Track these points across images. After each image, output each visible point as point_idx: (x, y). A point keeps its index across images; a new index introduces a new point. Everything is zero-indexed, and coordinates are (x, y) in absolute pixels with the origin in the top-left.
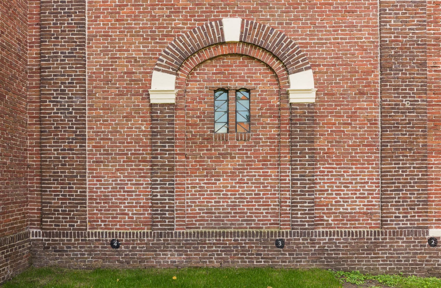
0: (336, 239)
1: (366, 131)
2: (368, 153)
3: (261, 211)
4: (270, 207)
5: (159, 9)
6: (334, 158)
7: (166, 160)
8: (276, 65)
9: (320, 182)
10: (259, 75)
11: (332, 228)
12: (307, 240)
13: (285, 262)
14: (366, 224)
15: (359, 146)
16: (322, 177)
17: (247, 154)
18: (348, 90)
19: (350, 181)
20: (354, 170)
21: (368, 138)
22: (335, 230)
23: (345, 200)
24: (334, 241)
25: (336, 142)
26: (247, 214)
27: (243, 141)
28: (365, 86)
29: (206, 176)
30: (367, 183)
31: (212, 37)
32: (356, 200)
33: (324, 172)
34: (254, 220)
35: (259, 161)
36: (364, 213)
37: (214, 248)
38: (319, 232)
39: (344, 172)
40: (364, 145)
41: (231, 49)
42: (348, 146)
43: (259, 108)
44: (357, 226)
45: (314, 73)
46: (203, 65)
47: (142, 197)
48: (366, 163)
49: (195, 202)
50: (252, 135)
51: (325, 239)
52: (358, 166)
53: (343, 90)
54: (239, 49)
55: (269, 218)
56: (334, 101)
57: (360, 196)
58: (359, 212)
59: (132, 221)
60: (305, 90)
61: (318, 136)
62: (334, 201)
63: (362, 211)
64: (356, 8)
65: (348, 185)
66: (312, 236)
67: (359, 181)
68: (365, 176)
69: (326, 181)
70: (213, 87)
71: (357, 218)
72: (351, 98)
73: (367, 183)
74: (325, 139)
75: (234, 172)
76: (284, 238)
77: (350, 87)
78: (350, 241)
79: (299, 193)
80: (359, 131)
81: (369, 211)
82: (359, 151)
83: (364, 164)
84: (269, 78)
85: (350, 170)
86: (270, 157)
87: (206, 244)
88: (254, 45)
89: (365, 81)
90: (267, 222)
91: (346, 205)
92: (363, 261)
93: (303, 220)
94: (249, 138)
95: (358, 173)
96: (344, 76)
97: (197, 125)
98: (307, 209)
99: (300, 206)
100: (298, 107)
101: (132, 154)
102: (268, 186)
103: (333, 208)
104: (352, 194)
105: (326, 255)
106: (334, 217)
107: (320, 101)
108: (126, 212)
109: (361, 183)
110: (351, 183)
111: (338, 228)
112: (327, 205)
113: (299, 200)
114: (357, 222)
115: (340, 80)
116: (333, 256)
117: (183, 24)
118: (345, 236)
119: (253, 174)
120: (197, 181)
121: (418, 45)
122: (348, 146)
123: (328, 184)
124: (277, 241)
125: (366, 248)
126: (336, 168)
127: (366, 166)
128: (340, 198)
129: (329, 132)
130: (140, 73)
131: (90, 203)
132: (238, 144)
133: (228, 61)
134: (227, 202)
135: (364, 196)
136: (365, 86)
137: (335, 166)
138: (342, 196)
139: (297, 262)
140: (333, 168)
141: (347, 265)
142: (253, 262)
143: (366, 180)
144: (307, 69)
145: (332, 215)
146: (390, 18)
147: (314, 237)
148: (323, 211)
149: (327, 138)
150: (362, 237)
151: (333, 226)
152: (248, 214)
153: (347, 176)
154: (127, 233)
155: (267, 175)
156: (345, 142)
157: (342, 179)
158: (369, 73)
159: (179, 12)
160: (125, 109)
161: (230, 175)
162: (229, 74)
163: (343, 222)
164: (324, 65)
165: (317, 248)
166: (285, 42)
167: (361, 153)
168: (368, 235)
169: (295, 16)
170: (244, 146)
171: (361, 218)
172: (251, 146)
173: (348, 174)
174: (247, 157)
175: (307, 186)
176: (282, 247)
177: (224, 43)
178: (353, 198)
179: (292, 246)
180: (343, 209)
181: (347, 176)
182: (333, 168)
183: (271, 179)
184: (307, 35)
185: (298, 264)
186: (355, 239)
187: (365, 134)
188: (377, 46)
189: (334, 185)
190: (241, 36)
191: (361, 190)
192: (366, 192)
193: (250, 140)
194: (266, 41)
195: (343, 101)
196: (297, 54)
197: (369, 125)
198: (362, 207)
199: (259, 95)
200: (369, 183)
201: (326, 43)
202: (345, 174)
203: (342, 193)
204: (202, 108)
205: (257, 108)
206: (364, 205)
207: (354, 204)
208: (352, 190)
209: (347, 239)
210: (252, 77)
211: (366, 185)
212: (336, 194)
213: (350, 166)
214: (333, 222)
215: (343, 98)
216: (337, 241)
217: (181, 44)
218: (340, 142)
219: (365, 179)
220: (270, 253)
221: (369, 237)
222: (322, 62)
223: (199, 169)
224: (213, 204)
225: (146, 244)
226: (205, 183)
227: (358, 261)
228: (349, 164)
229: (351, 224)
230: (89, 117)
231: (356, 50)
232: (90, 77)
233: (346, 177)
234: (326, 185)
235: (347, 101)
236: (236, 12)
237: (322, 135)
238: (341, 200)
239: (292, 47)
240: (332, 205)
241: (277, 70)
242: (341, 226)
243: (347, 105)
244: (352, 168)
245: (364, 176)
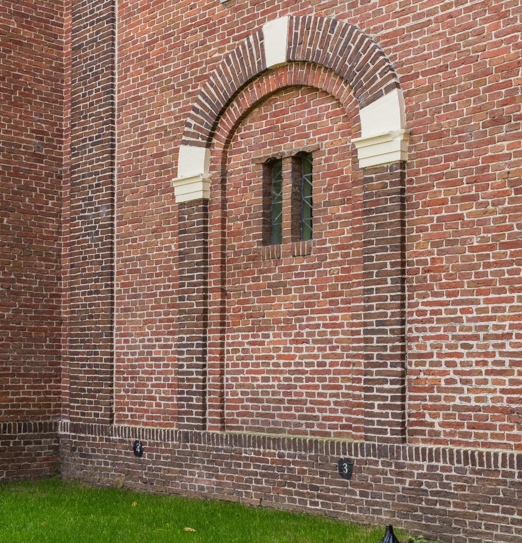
0: (443, 469)
1: (506, 210)
2: (510, 263)
3: (326, 400)
4: (340, 391)
6: (444, 281)
7: (194, 302)
9: (418, 337)
10: (325, 119)
11: (440, 442)
12: (389, 465)
13: (354, 509)
14: (510, 437)
15: (492, 247)
16: (420, 325)
17: (306, 282)
18: (470, 120)
19: (473, 332)
20: (482, 305)
21: (511, 228)
22: (47, 421)
23: (464, 377)
24: (438, 472)
25: (450, 243)
26: (306, 404)
27: (301, 257)
28: (504, 103)
29: (252, 329)
30: (509, 336)
31: (250, 65)
32: (487, 377)
33: (424, 313)
34: (316, 418)
35: (325, 296)
36: (504, 411)
37: (252, 469)
38: (417, 449)
39: (463, 311)
40: (504, 246)
41: (279, 79)
42: (472, 249)
43: (325, 186)
44: (490, 440)
46: (248, 119)
47: (170, 368)
48: (507, 287)
49: (236, 379)
50: (314, 245)
51: (421, 467)
52: (491, 296)
53: (462, 122)
54: (287, 79)
55: (340, 414)
56: (443, 150)
57: (495, 368)
58: (493, 407)
59: (159, 412)
60: (380, 137)
61: (415, 234)
62: (443, 378)
63: (499, 405)
65: (470, 342)
66: (398, 458)
67: (491, 332)
68: (503, 321)
69: (428, 334)
70: (260, 159)
71: (489, 421)
72: (477, 136)
73: (509, 336)
74: (427, 240)
75: (288, 319)
76: (353, 457)
77: (475, 111)
78: (468, 475)
79: (375, 360)
80: (493, 212)
81: (514, 406)
82: (492, 260)
83: (503, 291)
84: (341, 123)
85: (474, 307)
86: (343, 286)
87: (240, 458)
89: (503, 91)
90: (336, 423)
91: (466, 390)
92: (495, 528)
93: (383, 419)
94: (309, 249)
95: (490, 314)
96: (462, 88)
97: (241, 233)
98: (389, 395)
99: (378, 390)
100: (374, 176)
101: (162, 294)
102: (338, 347)
103: (443, 395)
104: (477, 363)
105: (423, 503)
106: (446, 416)
107: (417, 156)
108: (153, 394)
109: (497, 337)
110: (476, 337)
111: (453, 442)
112: (430, 389)
113: (374, 377)
114: (489, 432)
115: (454, 100)
116: (438, 506)
118: (459, 462)
119: (316, 322)
120: (240, 339)
122: (472, 249)
123: (432, 341)
124: (341, 461)
125: (501, 495)
126: (447, 304)
127: (508, 294)
128: (456, 373)
129: (435, 222)
131: (118, 379)
132: (294, 264)
133: (281, 102)
134: (279, 380)
135: (504, 368)
136: (504, 103)
137: (444, 298)
138: (459, 368)
139: (374, 512)
140: (441, 304)
141: (465, 531)
142: (305, 503)
143: (507, 330)
144: (388, 89)
145: (441, 413)
147: (401, 461)
148: (423, 403)
149: (431, 236)
150: (493, 468)
151: (442, 437)
152: (309, 405)
153: (469, 320)
154: (153, 430)
155: (336, 324)
156: (464, 242)
157: (458, 328)
159: (213, 32)
161: (282, 327)
162: (284, 127)
163: (461, 430)
164: (424, 74)
165: (407, 486)
166: (353, 43)
167: (496, 264)
168: (504, 465)
170: (304, 267)
171: (498, 423)
172: (312, 267)
173: (470, 316)
174: (308, 289)
175: (389, 345)
176: (349, 476)
177: (267, 72)
178: (480, 373)
179: (365, 477)
180: (461, 399)
181: (469, 320)
182: (441, 304)
183: (344, 333)
185: (376, 516)
186: (479, 472)
187: (504, 219)
189: (444, 343)
191: (497, 354)
192: (507, 360)
193: (312, 255)
194: (325, 49)
195: (461, 147)
196: (373, 62)
197: (513, 195)
198: (498, 394)
199: (326, 160)
200: (514, 336)
201: (429, 22)
202: (464, 317)
203: (458, 360)
204: (247, 200)
205: (323, 187)
206: (503, 391)
207: (482, 386)
208: (479, 355)
209: (464, 471)
210: (315, 126)
211: (507, 342)
212: (448, 364)
213: (475, 297)
214: (441, 429)
215: (461, 139)
216: (444, 474)
217: (212, 90)
218: (455, 242)
219: (503, 327)
220: (331, 487)
221: (508, 469)
222: (421, 67)
223: (242, 316)
224: (260, 383)
225: (170, 451)
226: (250, 343)
227: (487, 527)
228: (471, 293)
229: (477, 436)
230: (118, 237)
231: (486, 21)
232: (120, 170)
233: (465, 324)
234: (428, 343)
235: (469, 146)
237: (421, 231)
238: (457, 378)
240: (440, 390)
242: (457, 438)
243: (470, 154)
244: (477, 302)
245: (503, 319)
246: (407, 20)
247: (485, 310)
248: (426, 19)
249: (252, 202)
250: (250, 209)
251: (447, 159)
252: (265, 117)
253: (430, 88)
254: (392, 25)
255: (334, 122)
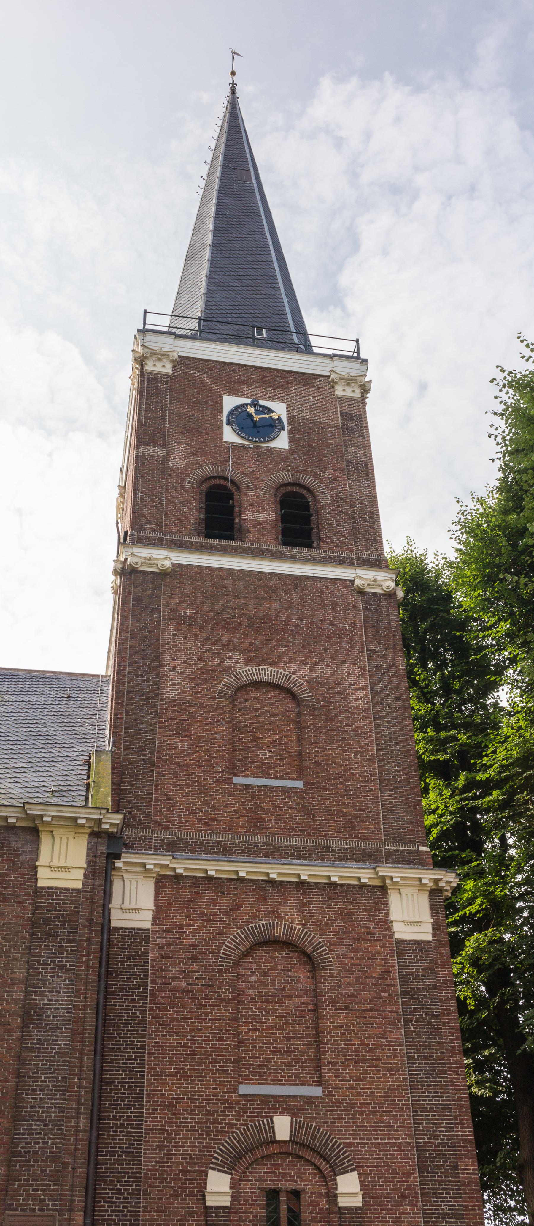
5: (214, 1103)
8: (323, 1165)
28: (406, 1189)
41: (282, 1147)
45: (359, 1174)
54: (290, 1148)
64: (392, 1108)
88: (302, 1145)
117: (236, 1120)
121: (449, 1147)
130: (195, 1171)
136: (406, 1189)
144: (352, 1170)
146: (422, 1119)
158: (408, 1175)
160: (179, 1212)
169: (338, 1115)
184: (350, 1135)
188: (413, 1147)
190: (291, 1135)
195: (388, 1205)
196: (343, 1154)
199: (309, 1197)
217: (235, 1142)
231: (395, 1151)
236: (285, 1109)
239: (338, 1148)
241: (325, 1170)
243: (391, 1209)
246: (356, 1139)
247: (122, 1140)
248: (366, 1141)
249: (257, 1213)
250: (257, 1217)
251: (381, 1209)
252: (267, 1165)
253: (370, 1174)
254: (349, 1139)
255: (314, 1177)
